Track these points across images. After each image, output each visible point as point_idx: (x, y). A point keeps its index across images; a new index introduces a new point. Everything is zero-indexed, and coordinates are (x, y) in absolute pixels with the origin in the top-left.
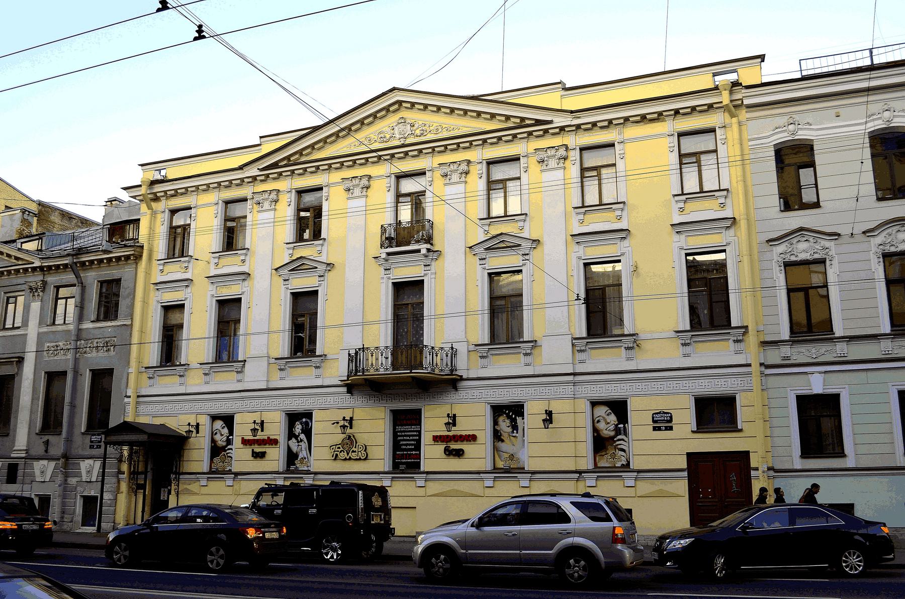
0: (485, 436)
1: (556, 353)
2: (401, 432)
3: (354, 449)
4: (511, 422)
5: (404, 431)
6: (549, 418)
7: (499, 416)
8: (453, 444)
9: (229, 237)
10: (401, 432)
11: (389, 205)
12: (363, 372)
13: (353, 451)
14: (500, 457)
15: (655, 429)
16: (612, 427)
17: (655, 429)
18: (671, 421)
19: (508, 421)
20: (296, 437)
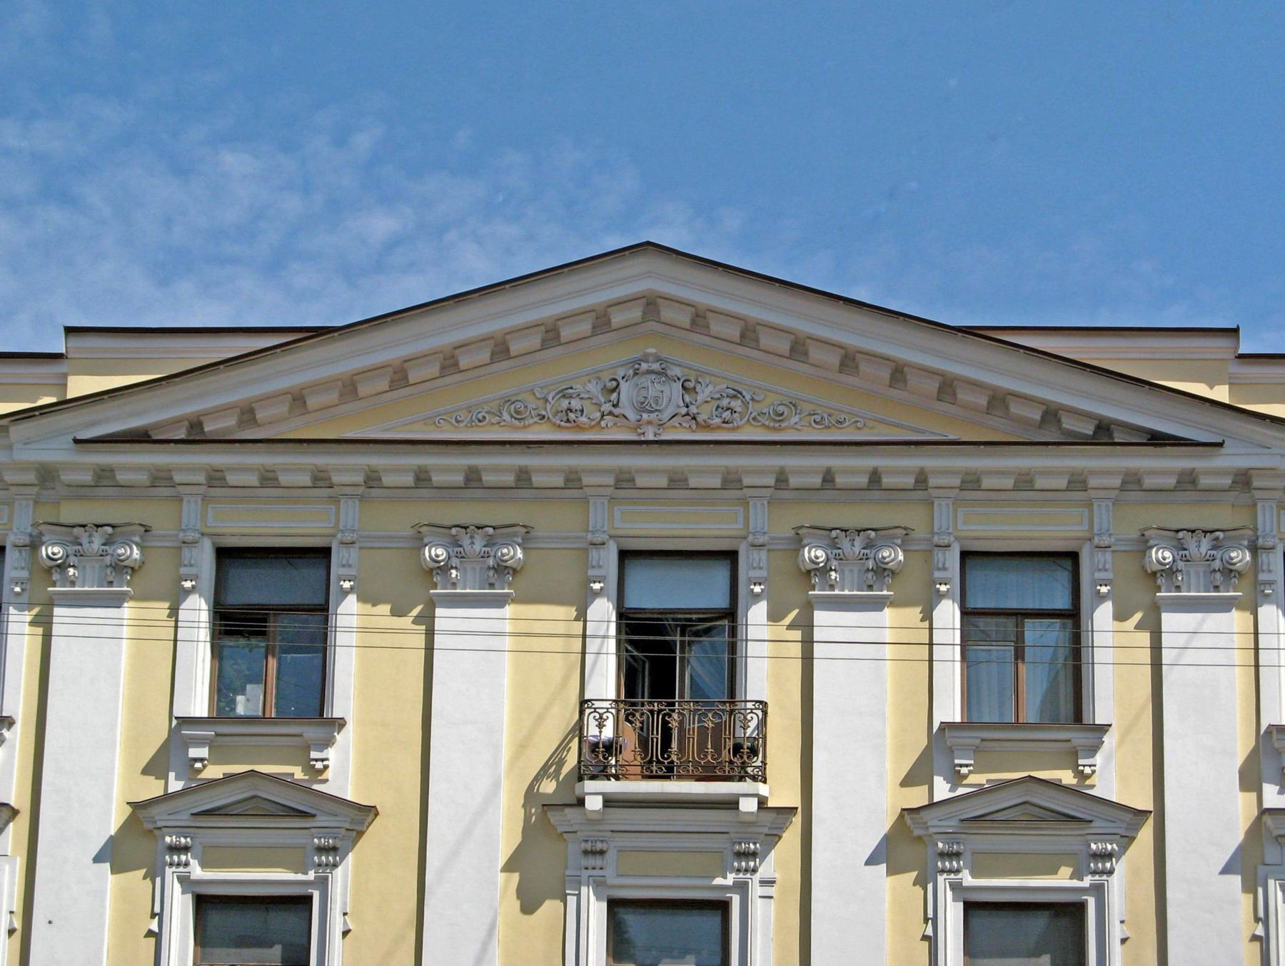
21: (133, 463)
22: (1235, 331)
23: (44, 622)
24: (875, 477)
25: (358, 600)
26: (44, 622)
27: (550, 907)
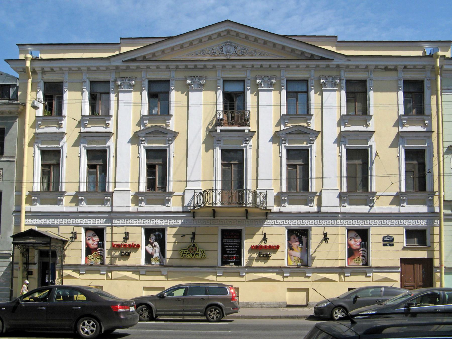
0: (284, 247)
1: (331, 202)
2: (226, 242)
3: (197, 252)
4: (299, 239)
5: (229, 243)
6: (326, 238)
7: (291, 235)
8: (264, 252)
9: (59, 104)
10: (226, 242)
11: (337, 105)
12: (246, 205)
13: (196, 254)
14: (291, 259)
15: (384, 245)
16: (96, 243)
17: (384, 245)
18: (393, 241)
19: (297, 238)
20: (152, 244)
21: (133, 65)
23: (117, 96)
26: (117, 96)
27: (211, 151)
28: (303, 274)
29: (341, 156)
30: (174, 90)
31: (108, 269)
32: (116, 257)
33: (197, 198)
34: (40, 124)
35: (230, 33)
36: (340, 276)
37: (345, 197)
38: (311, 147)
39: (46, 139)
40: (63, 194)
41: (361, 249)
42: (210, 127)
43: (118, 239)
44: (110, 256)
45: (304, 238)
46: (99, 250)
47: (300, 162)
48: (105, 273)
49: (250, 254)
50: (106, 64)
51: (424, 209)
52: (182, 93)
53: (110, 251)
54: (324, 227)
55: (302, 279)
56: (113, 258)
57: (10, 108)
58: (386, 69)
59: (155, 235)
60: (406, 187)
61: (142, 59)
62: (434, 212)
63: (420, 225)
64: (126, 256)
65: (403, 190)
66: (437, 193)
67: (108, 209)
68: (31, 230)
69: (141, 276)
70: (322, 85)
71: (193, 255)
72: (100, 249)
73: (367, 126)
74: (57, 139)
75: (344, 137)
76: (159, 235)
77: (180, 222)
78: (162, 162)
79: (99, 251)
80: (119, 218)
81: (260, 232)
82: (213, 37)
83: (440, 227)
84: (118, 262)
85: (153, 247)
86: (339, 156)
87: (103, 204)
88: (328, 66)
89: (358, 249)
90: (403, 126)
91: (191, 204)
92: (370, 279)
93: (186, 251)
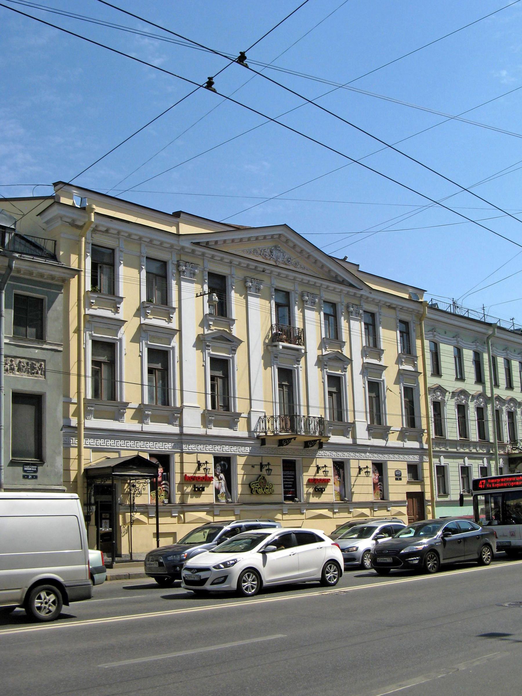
3: (267, 486)
13: (267, 488)
18: (401, 475)
21: (199, 250)
22: (358, 265)
23: (303, 312)
24: (256, 267)
25: (235, 292)
26: (303, 312)
27: (269, 368)
28: (230, 512)
29: (141, 357)
30: (122, 265)
31: (181, 510)
32: (188, 494)
33: (269, 422)
34: (93, 303)
35: (283, 238)
36: (371, 510)
37: (91, 407)
38: (233, 358)
39: (101, 325)
40: (388, 429)
41: (164, 482)
42: (267, 341)
43: (190, 470)
44: (180, 493)
45: (341, 471)
46: (163, 484)
47: (159, 366)
48: (177, 515)
49: (307, 489)
50: (172, 241)
51: (415, 445)
52: (241, 296)
53: (181, 484)
54: (359, 459)
55: (346, 515)
56: (183, 494)
57: (64, 273)
58: (390, 307)
59: (221, 465)
60: (151, 397)
61: (205, 245)
62: (70, 427)
63: (149, 449)
64: (198, 491)
65: (146, 402)
66: (426, 431)
67: (175, 430)
68: (138, 458)
69: (215, 518)
70: (247, 288)
71: (263, 490)
72: (164, 482)
73: (380, 359)
74: (115, 327)
75: (145, 331)
76: (224, 465)
77: (248, 449)
78: (223, 375)
79: (164, 486)
80: (189, 443)
81: (314, 464)
82: (267, 238)
83: (79, 447)
84: (191, 500)
85: (219, 480)
86: (203, 366)
87: (170, 423)
88: (355, 295)
89: (377, 483)
90: (146, 316)
91: (257, 429)
92: (351, 515)
93: (257, 485)
